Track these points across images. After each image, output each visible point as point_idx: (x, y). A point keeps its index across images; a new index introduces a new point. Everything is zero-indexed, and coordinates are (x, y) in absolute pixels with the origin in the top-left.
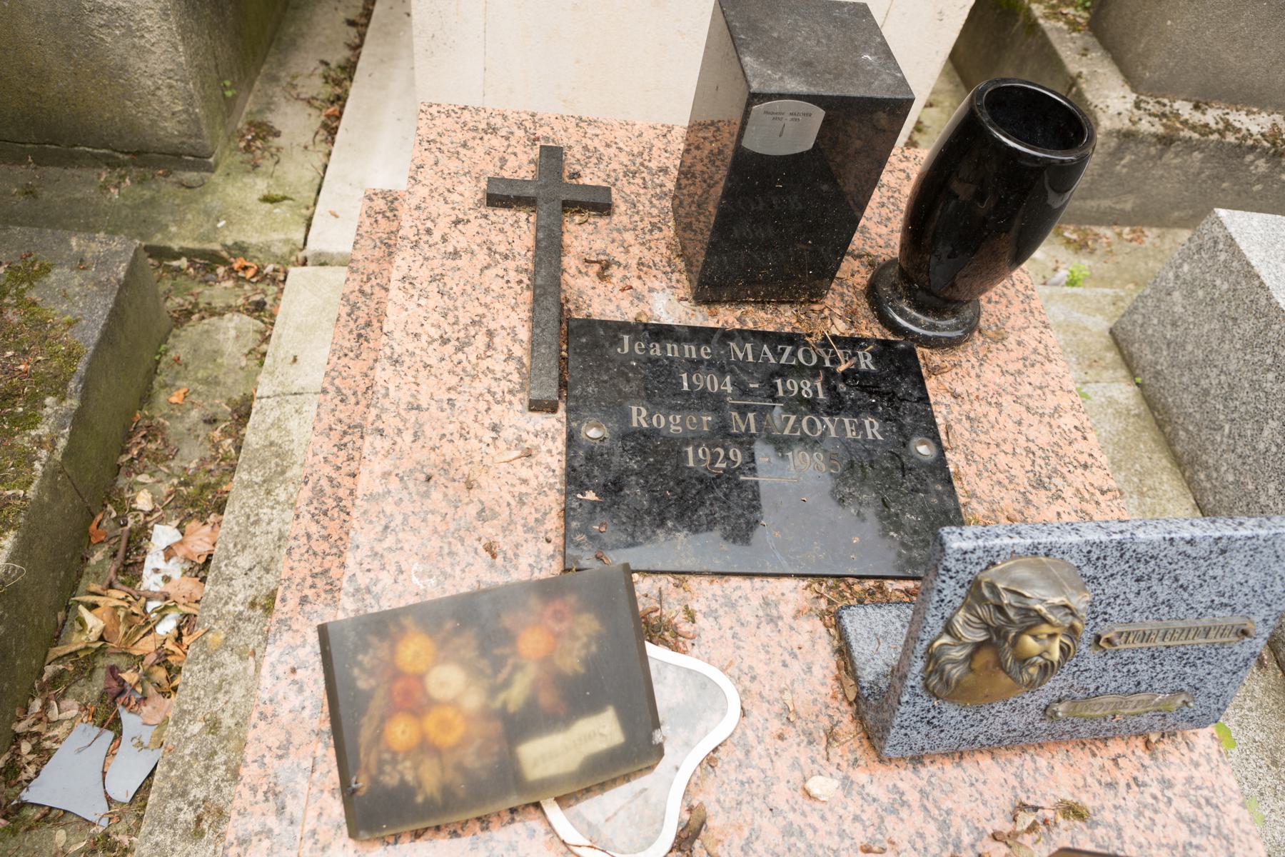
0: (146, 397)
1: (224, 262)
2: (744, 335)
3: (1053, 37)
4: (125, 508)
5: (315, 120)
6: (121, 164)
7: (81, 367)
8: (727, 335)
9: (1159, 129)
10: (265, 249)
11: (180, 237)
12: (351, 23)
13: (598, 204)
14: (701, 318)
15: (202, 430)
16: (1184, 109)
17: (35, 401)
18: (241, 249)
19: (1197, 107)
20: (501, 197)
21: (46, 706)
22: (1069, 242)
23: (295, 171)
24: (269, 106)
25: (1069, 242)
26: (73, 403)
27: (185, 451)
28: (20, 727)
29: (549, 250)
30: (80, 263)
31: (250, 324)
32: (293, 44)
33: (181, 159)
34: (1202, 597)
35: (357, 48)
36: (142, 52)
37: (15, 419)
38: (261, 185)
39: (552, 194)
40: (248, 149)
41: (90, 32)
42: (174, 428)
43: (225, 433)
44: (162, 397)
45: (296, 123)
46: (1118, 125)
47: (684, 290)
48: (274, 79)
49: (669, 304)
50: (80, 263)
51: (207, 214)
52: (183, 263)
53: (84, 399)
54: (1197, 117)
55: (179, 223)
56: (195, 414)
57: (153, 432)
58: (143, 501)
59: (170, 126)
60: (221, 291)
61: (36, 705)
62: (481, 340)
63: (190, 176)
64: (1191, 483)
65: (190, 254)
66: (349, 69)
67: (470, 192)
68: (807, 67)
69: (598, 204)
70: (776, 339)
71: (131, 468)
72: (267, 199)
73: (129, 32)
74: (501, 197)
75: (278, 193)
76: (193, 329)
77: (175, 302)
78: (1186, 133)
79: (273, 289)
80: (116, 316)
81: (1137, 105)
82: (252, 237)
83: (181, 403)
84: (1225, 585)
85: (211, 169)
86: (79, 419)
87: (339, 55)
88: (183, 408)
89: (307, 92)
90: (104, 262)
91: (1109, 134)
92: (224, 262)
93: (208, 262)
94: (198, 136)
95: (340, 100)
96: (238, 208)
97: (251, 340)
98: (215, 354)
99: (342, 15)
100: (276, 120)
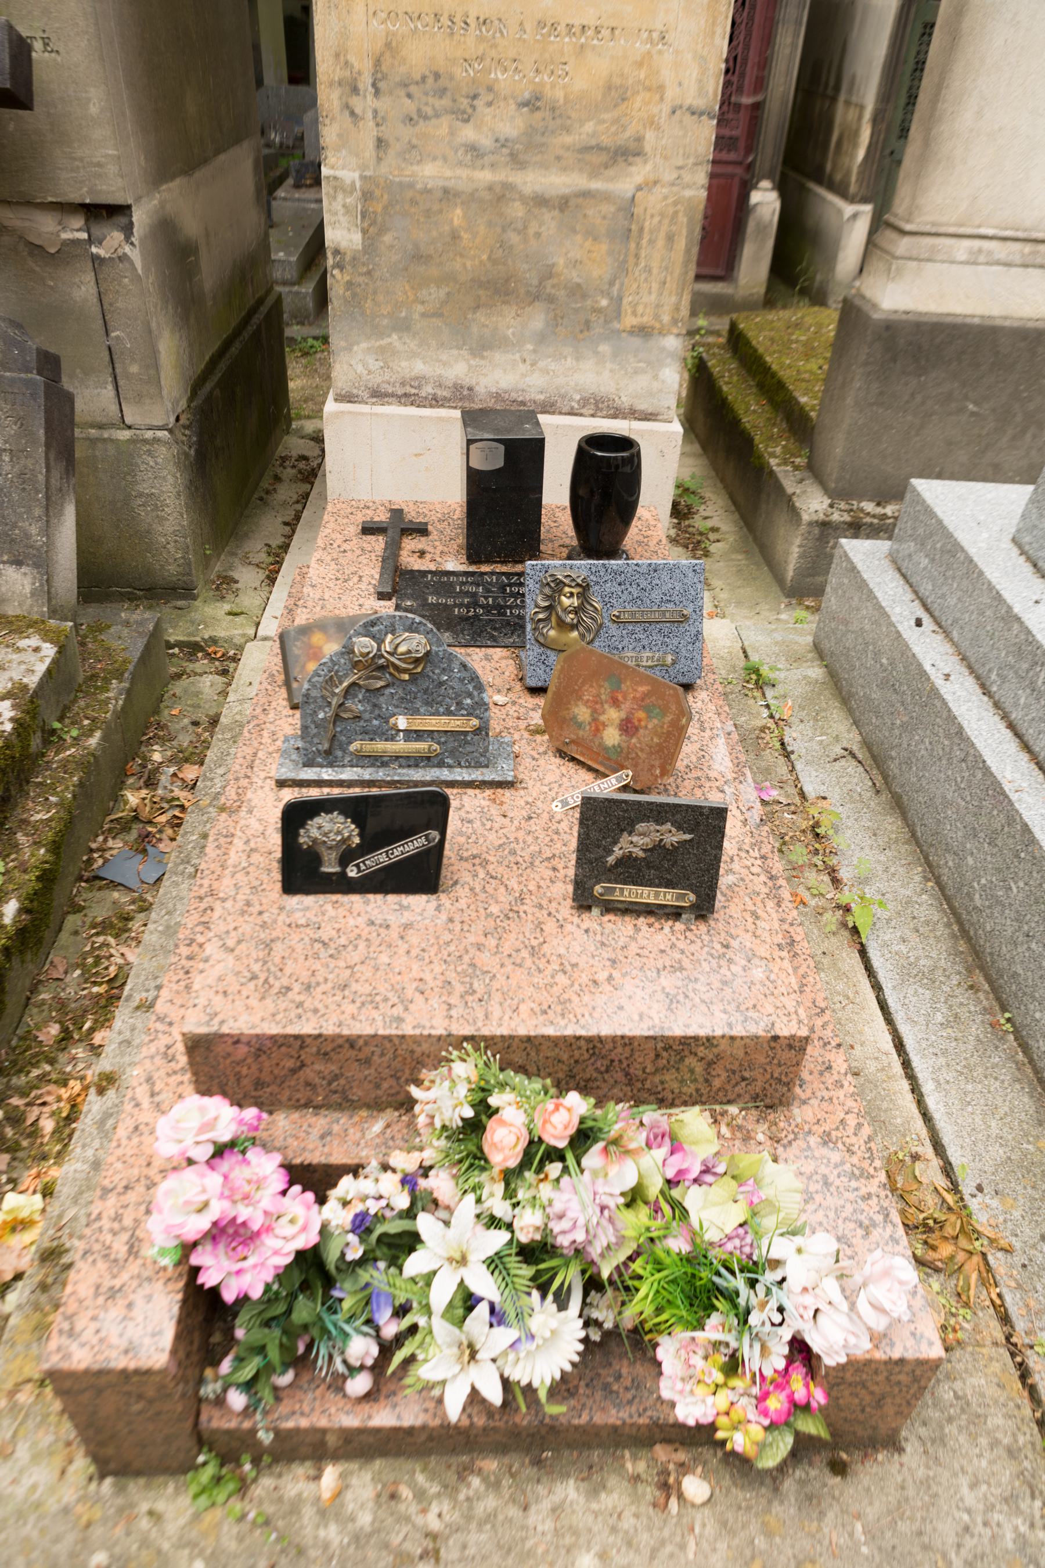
0: (157, 711)
1: (202, 649)
2: (492, 573)
3: (781, 476)
4: (146, 760)
5: (262, 575)
6: (139, 598)
7: (131, 667)
8: (482, 574)
9: (847, 518)
10: (229, 640)
11: (174, 635)
12: (286, 524)
13: (422, 531)
14: (472, 568)
15: (191, 728)
16: (869, 506)
17: (107, 681)
18: (214, 641)
19: (878, 504)
20: (368, 530)
21: (105, 840)
22: (808, 608)
23: (249, 600)
24: (231, 567)
25: (808, 608)
26: (126, 685)
27: (180, 737)
28: (94, 846)
29: (392, 552)
30: (127, 624)
31: (220, 680)
32: (246, 535)
33: (178, 592)
34: (656, 595)
35: (290, 537)
36: (161, 520)
37: (97, 688)
38: (227, 607)
39: (398, 528)
40: (217, 589)
41: (133, 510)
42: (174, 727)
43: (205, 730)
44: (166, 712)
45: (248, 577)
46: (815, 518)
47: (464, 559)
48: (234, 554)
49: (452, 565)
50: (127, 624)
51: (192, 622)
52: (176, 650)
53: (132, 683)
54: (879, 510)
55: (174, 627)
56: (186, 721)
57: (160, 726)
58: (157, 757)
59: (172, 569)
60: (201, 664)
61: (101, 838)
62: (356, 579)
63: (180, 603)
64: (850, 711)
65: (179, 644)
66: (285, 547)
67: (353, 530)
68: (497, 430)
69: (422, 531)
70: (508, 575)
71: (149, 743)
72: (230, 614)
73: (156, 508)
74: (368, 530)
75: (236, 610)
76: (184, 682)
77: (173, 670)
78: (868, 520)
79: (233, 665)
80: (148, 649)
81: (831, 506)
82: (221, 633)
83: (176, 714)
84: (664, 588)
85: (195, 598)
86: (129, 692)
87: (276, 541)
88: (182, 714)
89: (255, 561)
90: (141, 623)
91: (810, 524)
92: (202, 649)
93: (193, 649)
94: (189, 574)
95: (280, 563)
96: (212, 619)
97: (220, 688)
98: (197, 694)
99: (280, 520)
100: (236, 575)
